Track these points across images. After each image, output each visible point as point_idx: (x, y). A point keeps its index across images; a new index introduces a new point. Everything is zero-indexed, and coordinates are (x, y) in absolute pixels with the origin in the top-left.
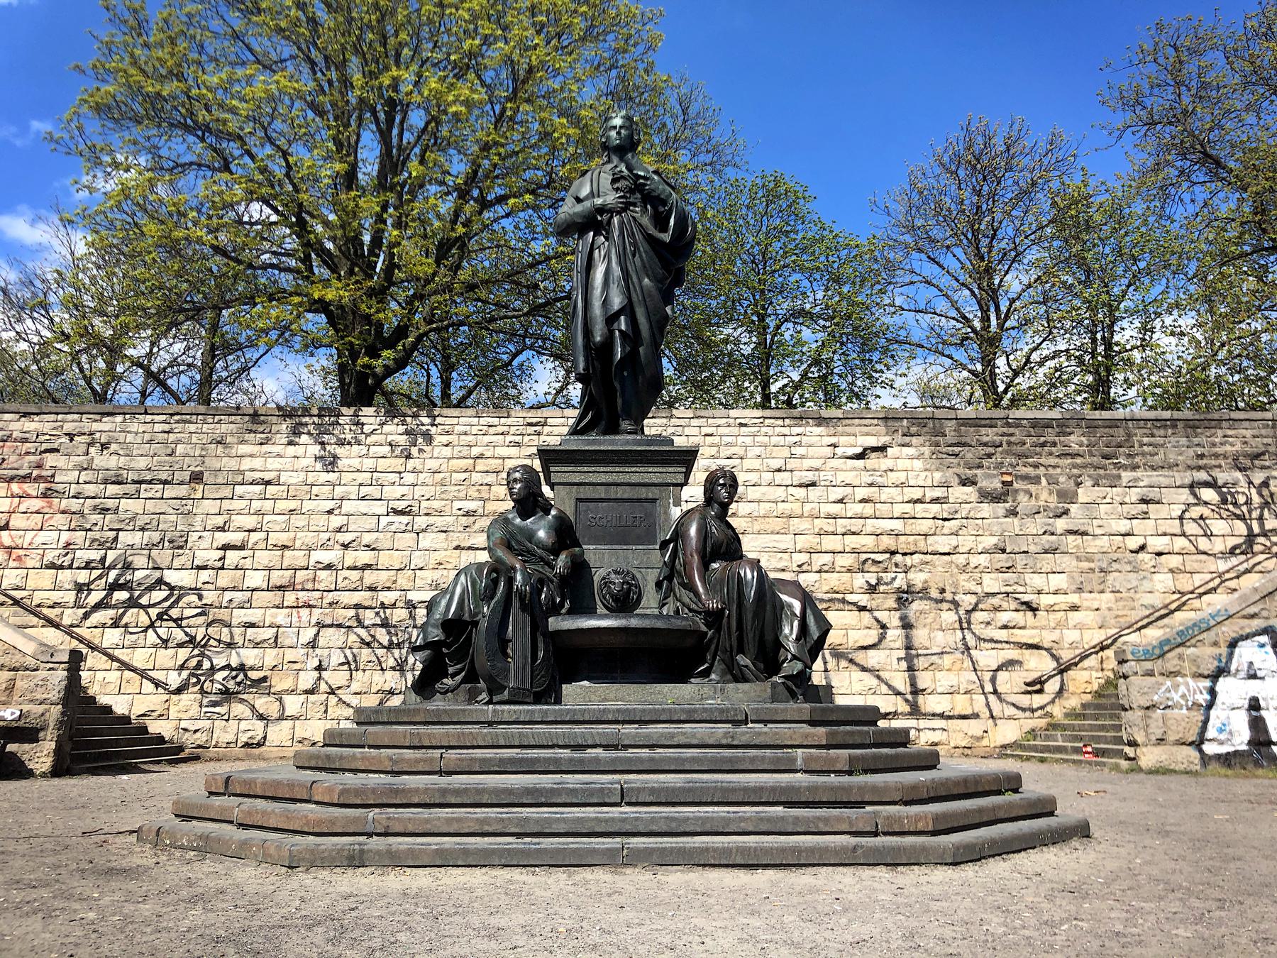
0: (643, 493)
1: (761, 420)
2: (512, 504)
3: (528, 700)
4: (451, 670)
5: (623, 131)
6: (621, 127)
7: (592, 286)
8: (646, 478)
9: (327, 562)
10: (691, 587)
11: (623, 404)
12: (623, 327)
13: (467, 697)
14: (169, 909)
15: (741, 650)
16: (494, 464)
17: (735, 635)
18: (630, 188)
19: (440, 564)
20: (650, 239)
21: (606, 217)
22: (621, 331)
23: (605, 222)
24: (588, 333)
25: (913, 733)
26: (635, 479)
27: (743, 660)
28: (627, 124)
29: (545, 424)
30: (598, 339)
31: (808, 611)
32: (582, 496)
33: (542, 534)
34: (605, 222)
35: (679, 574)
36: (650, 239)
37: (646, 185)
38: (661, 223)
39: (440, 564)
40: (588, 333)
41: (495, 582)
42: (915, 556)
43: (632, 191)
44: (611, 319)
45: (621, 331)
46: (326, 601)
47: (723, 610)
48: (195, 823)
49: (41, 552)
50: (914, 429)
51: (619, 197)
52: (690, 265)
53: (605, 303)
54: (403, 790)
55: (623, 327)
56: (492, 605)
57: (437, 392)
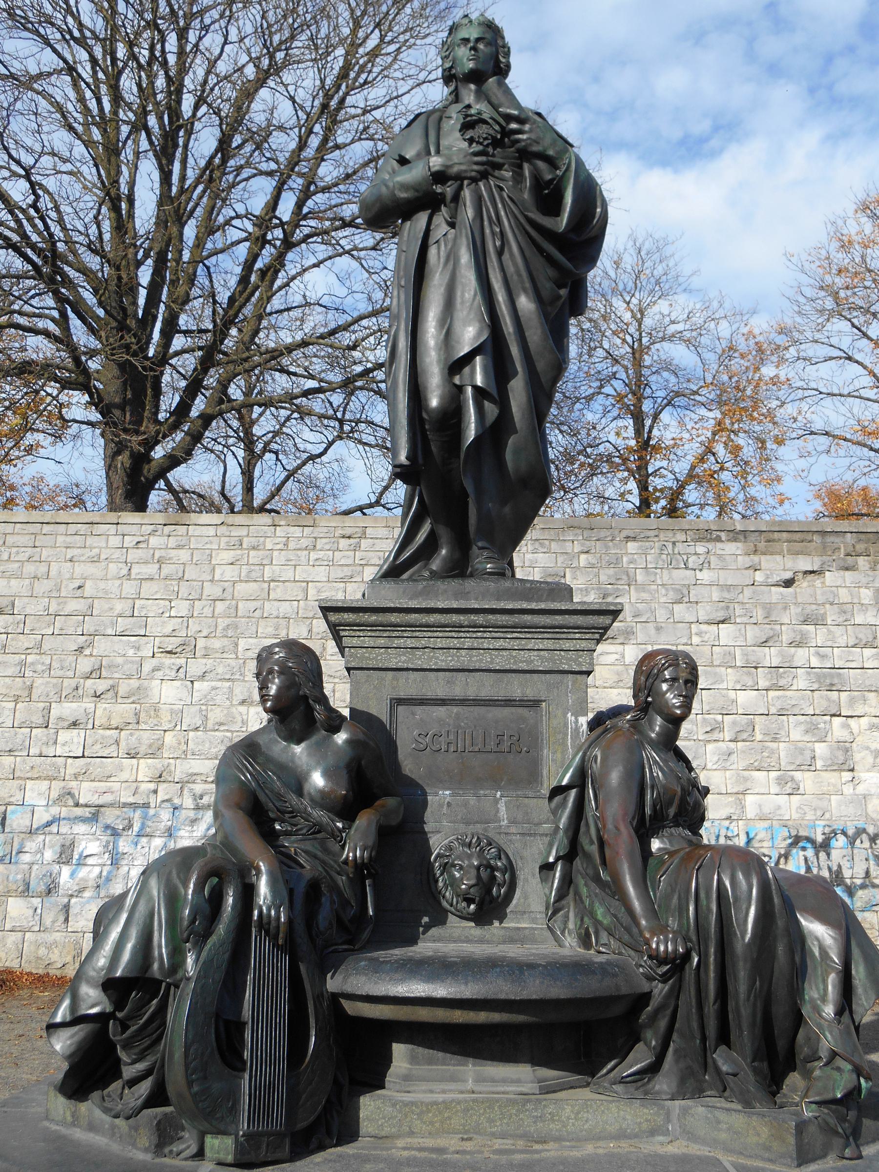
0: (516, 688)
1: (656, 532)
2: (265, 717)
3: (278, 1155)
4: (128, 1072)
5: (481, 46)
6: (478, 40)
8: (522, 661)
9: (72, 720)
10: (616, 890)
11: (480, 519)
12: (479, 381)
13: (155, 1139)
15: (724, 1038)
16: (295, 591)
17: (711, 1009)
18: (494, 138)
19: (221, 724)
21: (449, 190)
22: (475, 388)
23: (449, 197)
26: (500, 661)
27: (724, 1061)
28: (488, 36)
29: (363, 536)
30: (434, 402)
31: (856, 952)
33: (318, 779)
34: (449, 197)
35: (588, 856)
39: (221, 724)
41: (216, 900)
42: (863, 720)
43: (496, 143)
45: (475, 388)
46: (70, 771)
47: (686, 957)
49: (208, 552)
50: (860, 547)
51: (476, 154)
52: (594, 276)
53: (448, 338)
55: (479, 381)
56: (204, 954)
57: (236, 493)
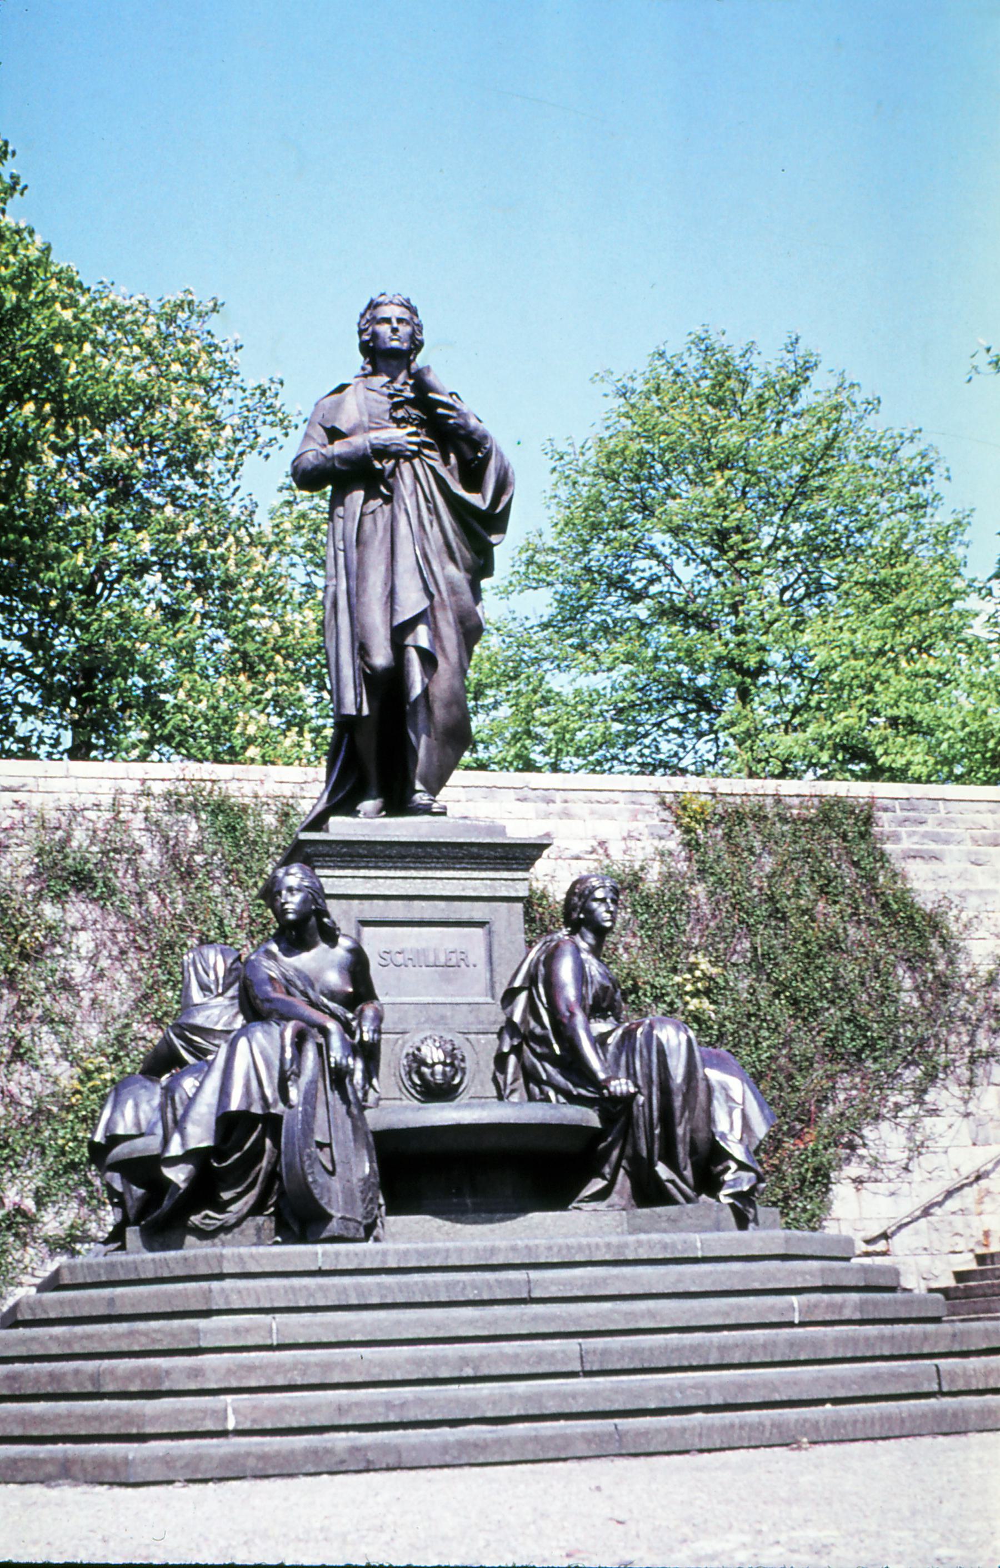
0: (477, 911)
7: (385, 610)
14: (838, 1068)
20: (455, 504)
21: (389, 465)
22: (420, 650)
24: (362, 650)
25: (885, 823)
32: (368, 916)
36: (455, 504)
37: (450, 417)
38: (473, 479)
40: (362, 650)
44: (399, 634)
45: (420, 650)
47: (635, 1095)
48: (153, 1444)
51: (410, 434)
54: (260, 1367)
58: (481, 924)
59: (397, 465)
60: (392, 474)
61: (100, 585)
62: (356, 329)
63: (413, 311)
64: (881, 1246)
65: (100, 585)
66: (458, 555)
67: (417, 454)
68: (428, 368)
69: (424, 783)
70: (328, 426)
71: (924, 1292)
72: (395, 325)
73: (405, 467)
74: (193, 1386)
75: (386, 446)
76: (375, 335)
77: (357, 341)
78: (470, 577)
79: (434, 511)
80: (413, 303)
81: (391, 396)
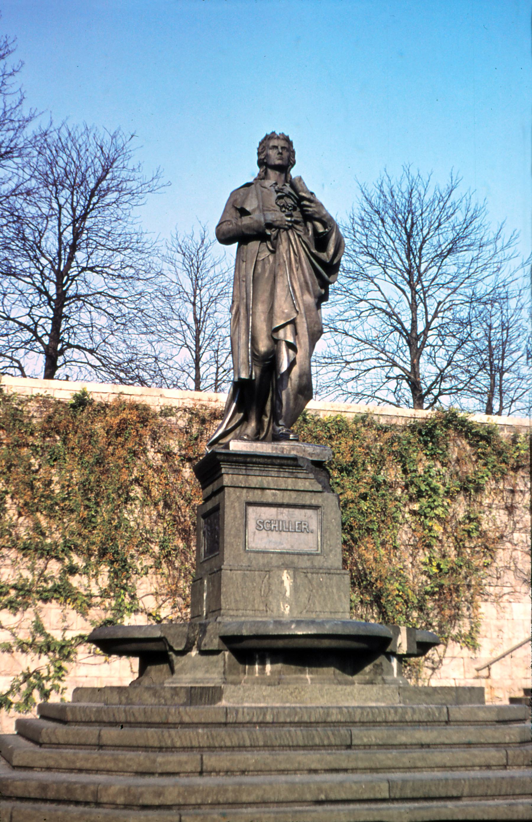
24: (254, 341)
32: (251, 499)
58: (316, 507)
59: (279, 232)
60: (276, 238)
61: (66, 278)
62: (256, 151)
63: (290, 143)
64: (485, 673)
65: (66, 278)
66: (311, 289)
67: (291, 227)
68: (300, 179)
69: (285, 421)
70: (239, 207)
71: (507, 702)
72: (280, 151)
73: (283, 235)
74: (157, 802)
75: (273, 221)
76: (267, 156)
77: (256, 158)
78: (317, 300)
79: (299, 261)
80: (291, 139)
81: (277, 192)
